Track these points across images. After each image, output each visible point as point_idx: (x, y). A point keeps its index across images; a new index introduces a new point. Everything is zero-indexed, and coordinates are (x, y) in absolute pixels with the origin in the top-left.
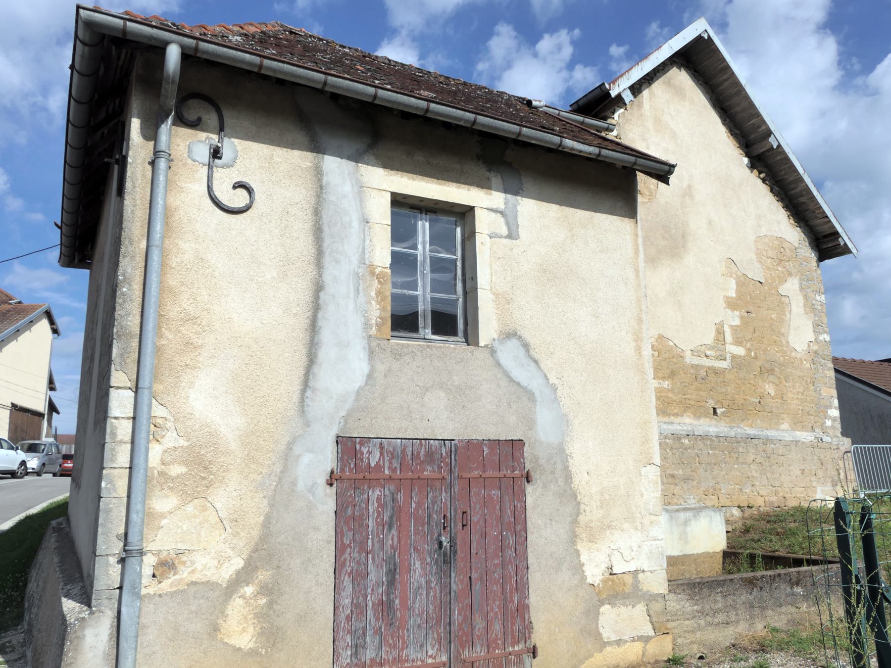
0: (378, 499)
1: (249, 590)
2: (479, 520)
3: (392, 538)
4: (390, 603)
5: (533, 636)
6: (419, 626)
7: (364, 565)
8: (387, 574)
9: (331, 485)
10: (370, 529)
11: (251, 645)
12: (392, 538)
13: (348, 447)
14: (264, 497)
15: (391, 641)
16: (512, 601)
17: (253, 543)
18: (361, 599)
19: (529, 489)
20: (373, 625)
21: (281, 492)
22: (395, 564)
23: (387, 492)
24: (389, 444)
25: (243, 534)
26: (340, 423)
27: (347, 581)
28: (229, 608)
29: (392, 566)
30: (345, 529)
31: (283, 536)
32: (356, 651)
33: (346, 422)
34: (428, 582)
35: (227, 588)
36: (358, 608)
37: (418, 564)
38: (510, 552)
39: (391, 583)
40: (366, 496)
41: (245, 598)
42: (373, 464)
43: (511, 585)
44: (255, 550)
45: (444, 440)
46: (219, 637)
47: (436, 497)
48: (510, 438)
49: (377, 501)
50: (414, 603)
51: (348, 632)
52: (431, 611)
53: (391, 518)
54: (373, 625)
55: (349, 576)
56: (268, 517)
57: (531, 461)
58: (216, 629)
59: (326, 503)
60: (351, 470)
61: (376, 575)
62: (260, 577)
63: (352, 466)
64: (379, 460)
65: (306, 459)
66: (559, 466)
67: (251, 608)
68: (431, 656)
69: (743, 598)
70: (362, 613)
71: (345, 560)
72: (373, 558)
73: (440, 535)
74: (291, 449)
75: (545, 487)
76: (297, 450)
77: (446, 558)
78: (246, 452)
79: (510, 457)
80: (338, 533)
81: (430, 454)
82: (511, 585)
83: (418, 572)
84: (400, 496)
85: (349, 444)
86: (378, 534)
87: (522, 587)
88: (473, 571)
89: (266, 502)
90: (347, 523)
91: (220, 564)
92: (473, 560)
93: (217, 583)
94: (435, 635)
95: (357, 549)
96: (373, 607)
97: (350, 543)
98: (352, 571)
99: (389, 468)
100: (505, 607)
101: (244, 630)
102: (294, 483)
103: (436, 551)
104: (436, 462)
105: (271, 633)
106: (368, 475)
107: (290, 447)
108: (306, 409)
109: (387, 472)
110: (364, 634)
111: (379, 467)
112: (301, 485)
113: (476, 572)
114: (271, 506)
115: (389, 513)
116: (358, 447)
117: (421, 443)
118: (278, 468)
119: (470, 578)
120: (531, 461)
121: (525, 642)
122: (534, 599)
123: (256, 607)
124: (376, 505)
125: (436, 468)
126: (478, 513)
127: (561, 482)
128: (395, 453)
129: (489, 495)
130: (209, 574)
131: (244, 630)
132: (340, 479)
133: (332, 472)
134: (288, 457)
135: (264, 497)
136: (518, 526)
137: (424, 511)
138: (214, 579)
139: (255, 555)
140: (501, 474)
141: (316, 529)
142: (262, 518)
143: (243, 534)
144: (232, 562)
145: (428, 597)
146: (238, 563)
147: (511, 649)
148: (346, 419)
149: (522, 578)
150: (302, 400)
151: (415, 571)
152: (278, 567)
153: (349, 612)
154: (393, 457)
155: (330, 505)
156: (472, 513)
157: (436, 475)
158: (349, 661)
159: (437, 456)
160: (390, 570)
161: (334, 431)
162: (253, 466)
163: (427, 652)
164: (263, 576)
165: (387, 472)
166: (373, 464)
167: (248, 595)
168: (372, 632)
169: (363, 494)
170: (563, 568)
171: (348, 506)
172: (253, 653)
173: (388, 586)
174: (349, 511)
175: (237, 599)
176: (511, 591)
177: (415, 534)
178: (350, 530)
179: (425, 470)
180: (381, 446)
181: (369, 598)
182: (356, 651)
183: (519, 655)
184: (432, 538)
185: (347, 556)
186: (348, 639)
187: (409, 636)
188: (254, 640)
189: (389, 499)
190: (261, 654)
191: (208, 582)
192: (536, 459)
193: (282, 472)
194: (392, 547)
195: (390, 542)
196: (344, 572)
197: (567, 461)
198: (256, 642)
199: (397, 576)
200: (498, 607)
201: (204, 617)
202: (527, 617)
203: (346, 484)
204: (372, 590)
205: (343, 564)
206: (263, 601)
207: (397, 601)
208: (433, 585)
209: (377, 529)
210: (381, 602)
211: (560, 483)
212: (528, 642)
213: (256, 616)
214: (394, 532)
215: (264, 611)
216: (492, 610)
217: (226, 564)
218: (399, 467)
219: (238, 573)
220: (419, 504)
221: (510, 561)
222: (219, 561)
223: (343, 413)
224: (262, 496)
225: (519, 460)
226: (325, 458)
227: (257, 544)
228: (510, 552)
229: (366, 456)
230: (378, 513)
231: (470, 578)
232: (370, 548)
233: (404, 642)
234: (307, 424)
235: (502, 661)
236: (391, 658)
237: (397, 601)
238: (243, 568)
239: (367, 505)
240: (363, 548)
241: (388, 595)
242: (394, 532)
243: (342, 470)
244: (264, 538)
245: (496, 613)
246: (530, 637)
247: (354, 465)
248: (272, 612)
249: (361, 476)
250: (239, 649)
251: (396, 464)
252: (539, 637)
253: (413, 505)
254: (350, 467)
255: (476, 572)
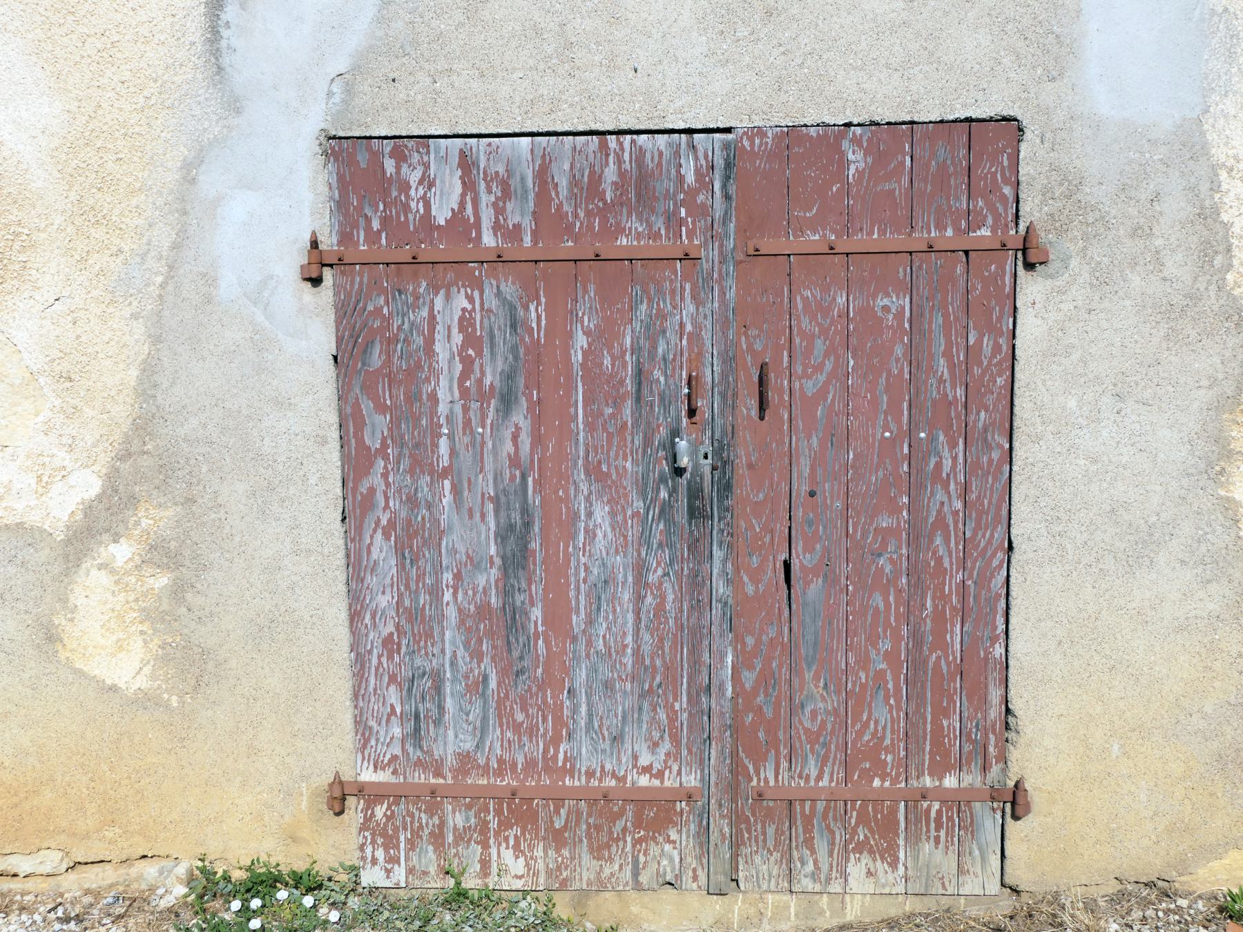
0: (465, 322)
1: (122, 552)
2: (822, 393)
3: (515, 438)
4: (513, 619)
5: (1014, 754)
6: (608, 685)
7: (429, 506)
8: (501, 538)
9: (316, 281)
10: (442, 409)
11: (142, 682)
12: (515, 438)
13: (361, 165)
14: (135, 316)
15: (520, 717)
16: (941, 643)
17: (117, 437)
18: (423, 599)
19: (1032, 288)
20: (463, 668)
21: (177, 297)
22: (525, 511)
23: (492, 302)
24: (492, 153)
25: (89, 412)
26: (330, 94)
27: (381, 550)
28: (78, 589)
29: (516, 517)
30: (367, 406)
31: (194, 422)
32: (417, 730)
33: (349, 90)
34: (640, 569)
35: (68, 542)
36: (418, 623)
37: (601, 513)
38: (940, 496)
39: (515, 561)
40: (425, 313)
41: (113, 572)
42: (441, 215)
43: (941, 597)
44: (126, 455)
45: (690, 131)
46: (63, 655)
47: (663, 316)
48: (962, 115)
49: (462, 329)
50: (590, 622)
51: (393, 679)
52: (646, 649)
53: (509, 376)
54: (463, 668)
55: (387, 536)
56: (149, 369)
57: (1047, 192)
58: (52, 636)
59: (307, 329)
60: (373, 238)
61: (471, 536)
62: (145, 523)
63: (376, 225)
64: (462, 204)
65: (238, 208)
66: (1175, 207)
67: (132, 597)
68: (647, 770)
69: (1164, 905)
70: (429, 635)
71: (372, 491)
72: (456, 490)
73: (675, 433)
74: (193, 181)
75: (1101, 281)
76: (211, 181)
77: (699, 503)
78: (73, 196)
79: (958, 183)
80: (350, 423)
81: (641, 186)
82: (941, 597)
83: (602, 534)
84: (535, 314)
85: (363, 158)
86: (467, 423)
87: (990, 609)
88: (798, 546)
89: (139, 328)
90: (369, 389)
91: (43, 485)
92: (799, 513)
93: (42, 531)
94: (662, 715)
95: (405, 464)
96: (462, 622)
97: (384, 445)
98: (392, 524)
99: (496, 227)
100: (917, 664)
101: (120, 646)
102: (209, 279)
103: (663, 479)
104: (660, 208)
105: (189, 664)
106: (426, 251)
107: (189, 174)
108: (226, 61)
109: (488, 240)
110: (438, 688)
111: (462, 226)
112: (228, 286)
113: (809, 548)
114: (156, 340)
115: (500, 365)
116: (389, 166)
117: (604, 147)
118: (163, 237)
119: (787, 566)
120: (1047, 192)
121: (985, 769)
122: (1028, 644)
123: (145, 595)
124: (458, 338)
125: (659, 224)
126: (819, 368)
127: (1178, 266)
128: (514, 183)
129: (867, 312)
130: (19, 506)
131: (120, 646)
132: (339, 263)
133: (315, 244)
134: (186, 204)
135: (135, 316)
136: (984, 413)
137: (618, 358)
138: (34, 519)
139: (125, 467)
140: (920, 238)
141: (283, 404)
142: (134, 372)
143: (89, 412)
144: (72, 480)
145: (637, 613)
146: (88, 485)
147: (928, 781)
148: (348, 81)
149: (984, 580)
150: (214, 34)
151: (591, 534)
152: (191, 501)
153: (390, 628)
154: (507, 194)
155: (319, 337)
156: (799, 369)
157: (665, 245)
158: (397, 751)
159: (664, 185)
160: (511, 527)
161: (315, 119)
162: (99, 233)
163: (635, 758)
164: (153, 518)
165: (488, 240)
166: (441, 215)
167: (120, 562)
168: (460, 688)
169: (415, 307)
170: (1161, 558)
171: (369, 344)
172: (145, 700)
173: (505, 568)
174: (376, 359)
175: (94, 572)
176: (939, 617)
177: (590, 427)
178: (381, 408)
179: (621, 230)
180: (466, 164)
181: (448, 596)
182: (417, 730)
183: (958, 802)
184: (647, 442)
185: (375, 479)
186: (393, 696)
187: (575, 710)
188: (147, 670)
189: (500, 320)
190: (167, 706)
191: (20, 525)
192: (1073, 185)
193: (175, 247)
194: (515, 461)
195: (509, 447)
196: (369, 524)
197: (1215, 187)
198: (153, 677)
199: (535, 545)
200: (890, 657)
201: (21, 606)
202: (995, 695)
203: (361, 277)
204: (458, 577)
205: (368, 502)
206: (162, 581)
207: (537, 613)
208: (652, 578)
209: (466, 409)
210: (484, 611)
211: (1171, 269)
212: (995, 769)
213: (147, 615)
214: (520, 417)
215: (165, 606)
216: (864, 662)
217: (58, 487)
218: (527, 223)
219: (89, 509)
220: (604, 336)
221: (940, 522)
222: (39, 477)
223: (341, 64)
224: (127, 312)
225: (994, 189)
226: (300, 204)
227: (127, 440)
228: (940, 496)
229: (416, 192)
230: (467, 363)
231: (787, 566)
232: (445, 462)
233: (559, 722)
234: (234, 106)
235: (894, 811)
236: (520, 760)
237: (537, 613)
238: (99, 498)
239: (430, 342)
240: (421, 463)
241: (507, 592)
242: (520, 417)
243: (346, 238)
244: (143, 426)
245: (880, 675)
246: (1003, 759)
247: (383, 228)
248: (183, 610)
249: (405, 254)
250: (114, 689)
251: (519, 214)
252: (1037, 757)
253: (581, 341)
254: (368, 228)
255: (809, 548)
